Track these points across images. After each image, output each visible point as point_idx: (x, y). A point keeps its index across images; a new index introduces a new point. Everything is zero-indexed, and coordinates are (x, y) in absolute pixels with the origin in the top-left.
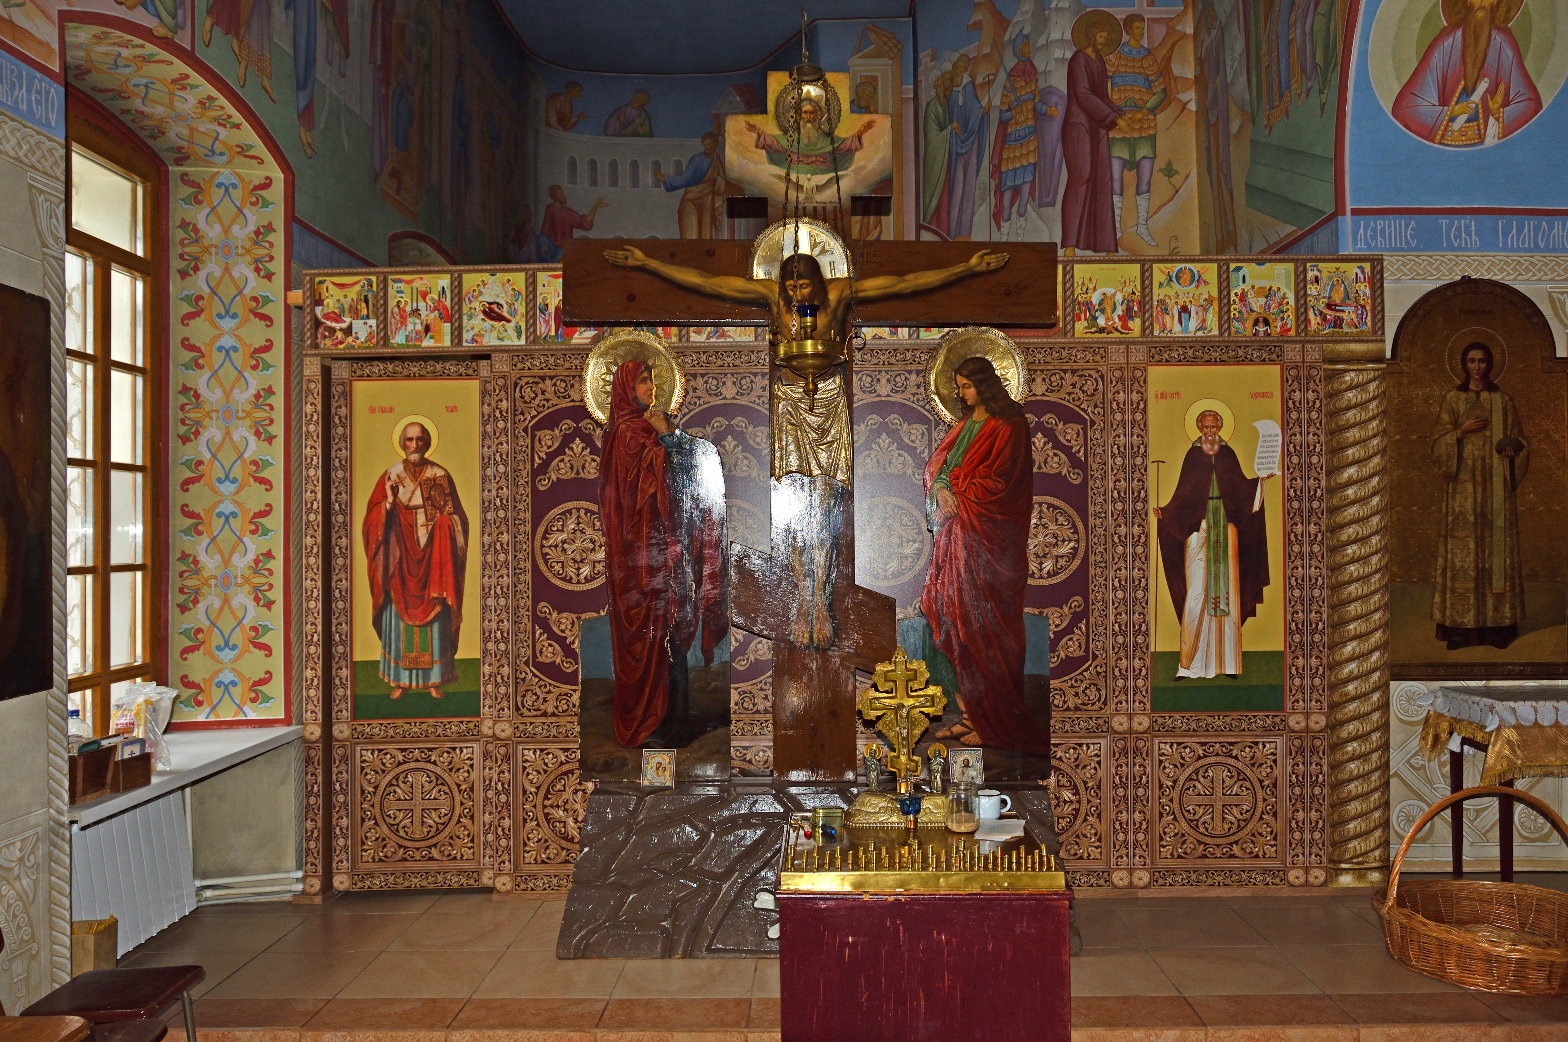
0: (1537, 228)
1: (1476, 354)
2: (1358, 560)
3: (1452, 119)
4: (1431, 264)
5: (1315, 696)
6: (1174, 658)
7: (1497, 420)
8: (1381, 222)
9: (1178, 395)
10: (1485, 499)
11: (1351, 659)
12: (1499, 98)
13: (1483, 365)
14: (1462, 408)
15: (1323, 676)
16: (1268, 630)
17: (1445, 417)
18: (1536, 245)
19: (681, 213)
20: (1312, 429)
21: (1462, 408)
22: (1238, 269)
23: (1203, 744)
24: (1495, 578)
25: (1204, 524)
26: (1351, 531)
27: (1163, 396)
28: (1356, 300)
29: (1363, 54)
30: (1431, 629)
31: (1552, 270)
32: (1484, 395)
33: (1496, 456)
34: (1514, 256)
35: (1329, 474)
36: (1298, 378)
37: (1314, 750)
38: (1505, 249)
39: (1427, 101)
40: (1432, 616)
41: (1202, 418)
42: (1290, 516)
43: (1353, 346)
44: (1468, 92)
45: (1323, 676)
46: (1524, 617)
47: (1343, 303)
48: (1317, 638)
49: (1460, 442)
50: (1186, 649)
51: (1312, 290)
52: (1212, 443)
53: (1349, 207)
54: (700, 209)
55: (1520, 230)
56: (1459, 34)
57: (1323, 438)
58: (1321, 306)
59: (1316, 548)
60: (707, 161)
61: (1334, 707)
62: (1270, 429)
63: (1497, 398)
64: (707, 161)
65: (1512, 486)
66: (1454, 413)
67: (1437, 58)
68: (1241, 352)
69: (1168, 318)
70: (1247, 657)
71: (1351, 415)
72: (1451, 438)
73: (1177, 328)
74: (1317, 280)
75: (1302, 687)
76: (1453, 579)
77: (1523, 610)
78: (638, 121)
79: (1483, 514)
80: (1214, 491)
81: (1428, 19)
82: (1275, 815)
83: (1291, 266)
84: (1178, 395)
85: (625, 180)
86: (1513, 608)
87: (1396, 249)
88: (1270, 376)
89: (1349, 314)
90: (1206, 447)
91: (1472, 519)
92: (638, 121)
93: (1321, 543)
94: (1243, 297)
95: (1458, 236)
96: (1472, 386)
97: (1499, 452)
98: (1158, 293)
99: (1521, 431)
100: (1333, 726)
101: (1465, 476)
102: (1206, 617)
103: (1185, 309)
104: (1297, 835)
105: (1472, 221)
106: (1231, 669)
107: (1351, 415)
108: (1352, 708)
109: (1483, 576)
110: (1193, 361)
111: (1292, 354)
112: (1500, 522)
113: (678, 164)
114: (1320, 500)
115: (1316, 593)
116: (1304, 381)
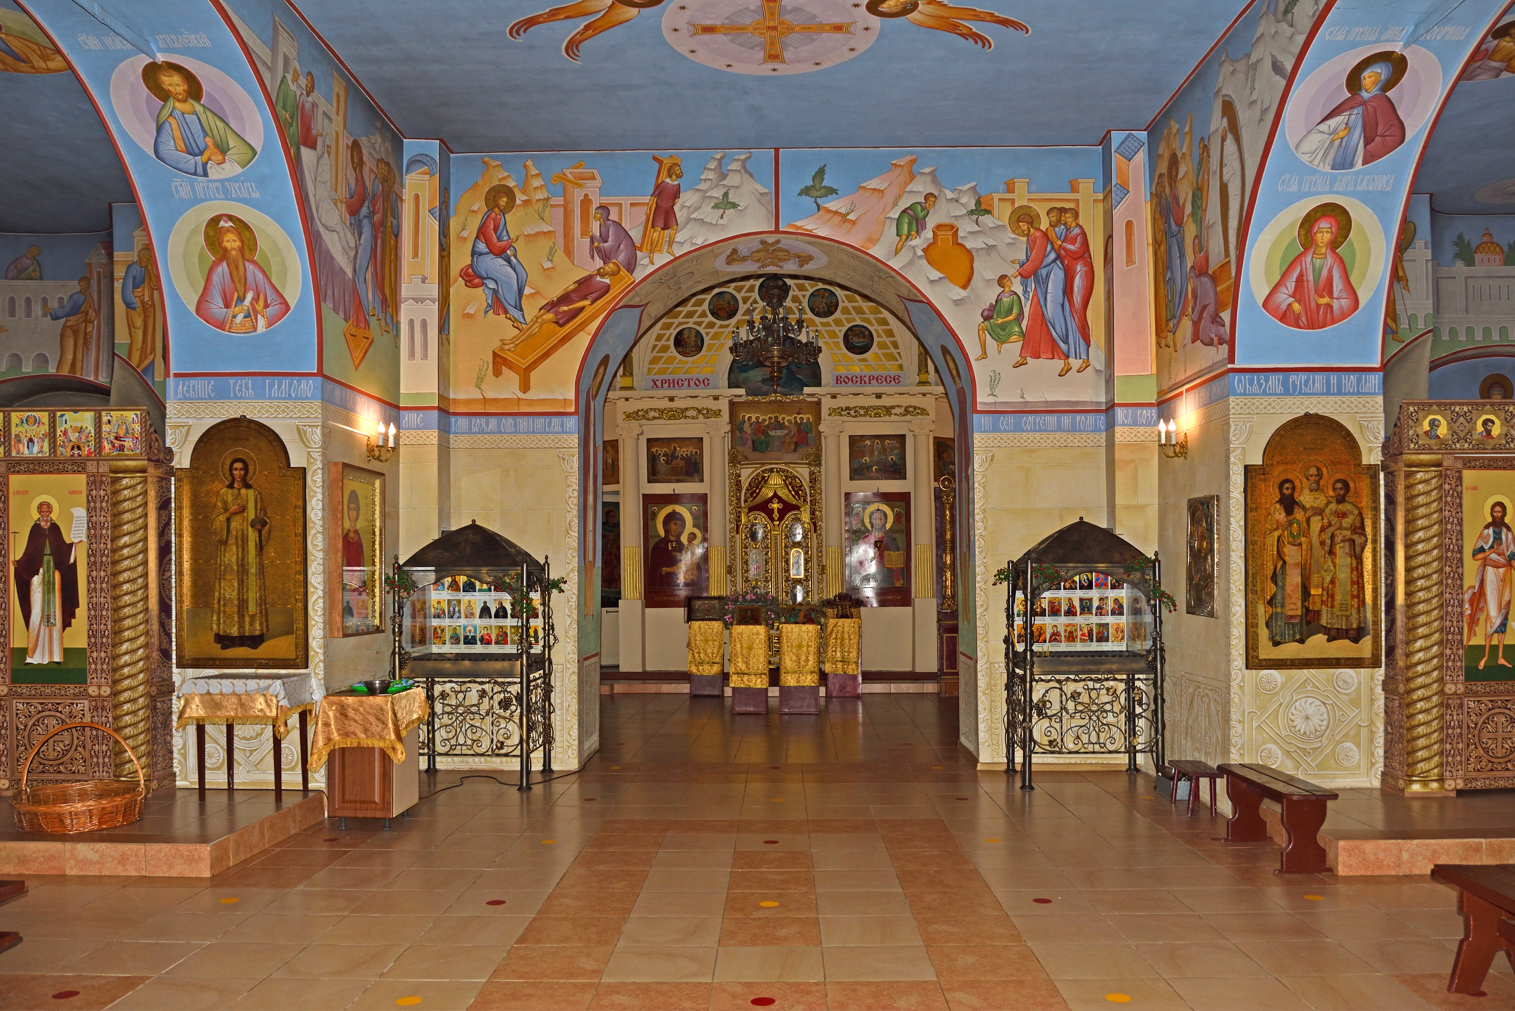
0: (290, 385)
1: (238, 465)
2: (130, 593)
3: (234, 317)
4: (223, 408)
5: (104, 675)
6: (23, 652)
7: (251, 506)
8: (193, 382)
9: (27, 492)
10: (243, 556)
11: (126, 653)
12: (261, 302)
13: (242, 472)
14: (230, 498)
15: (108, 663)
16: (78, 635)
17: (219, 504)
18: (290, 395)
19: (62, 336)
20: (103, 513)
21: (230, 498)
22: (62, 416)
23: (42, 704)
24: (250, 605)
25: (41, 571)
26: (126, 575)
27: (18, 493)
28: (133, 434)
29: (169, 278)
30: (211, 637)
31: (300, 411)
32: (243, 491)
33: (250, 529)
34: (275, 402)
35: (113, 540)
36: (94, 482)
37: (103, 708)
38: (270, 398)
39: (217, 305)
40: (211, 629)
41: (41, 506)
42: (91, 566)
43: (128, 463)
44: (241, 299)
45: (108, 663)
46: (268, 629)
47: (125, 436)
48: (105, 640)
49: (228, 520)
50: (31, 646)
51: (105, 428)
52: (46, 522)
53: (172, 372)
54: (76, 333)
55: (279, 386)
56: (225, 264)
57: (109, 519)
58: (112, 438)
59: (104, 586)
60: (82, 298)
61: (115, 682)
62: (80, 512)
63: (251, 492)
64: (82, 298)
65: (260, 548)
66: (225, 502)
67: (216, 278)
68: (61, 466)
69: (21, 446)
70: (66, 651)
71: (127, 505)
72: (222, 518)
73: (26, 451)
74: (109, 422)
75: (96, 670)
76: (225, 605)
77: (267, 625)
78: (31, 268)
79: (243, 566)
80: (48, 550)
81: (201, 256)
82: (84, 747)
83: (92, 413)
84: (27, 492)
85: (20, 311)
86: (261, 624)
87: (202, 399)
88: (81, 480)
89: (128, 443)
90: (43, 524)
91: (235, 568)
92: (31, 268)
93: (107, 582)
94: (65, 433)
95: (240, 390)
96: (236, 485)
97: (252, 526)
98: (14, 430)
99: (266, 513)
100: (115, 694)
101: (231, 541)
102: (43, 627)
103: (31, 440)
104: (95, 760)
105: (249, 380)
106: (57, 658)
107: (127, 505)
108: (127, 683)
109: (243, 604)
110: (33, 472)
111: (92, 467)
112: (253, 570)
113: (61, 300)
114: (107, 556)
115: (104, 613)
116: (98, 484)
